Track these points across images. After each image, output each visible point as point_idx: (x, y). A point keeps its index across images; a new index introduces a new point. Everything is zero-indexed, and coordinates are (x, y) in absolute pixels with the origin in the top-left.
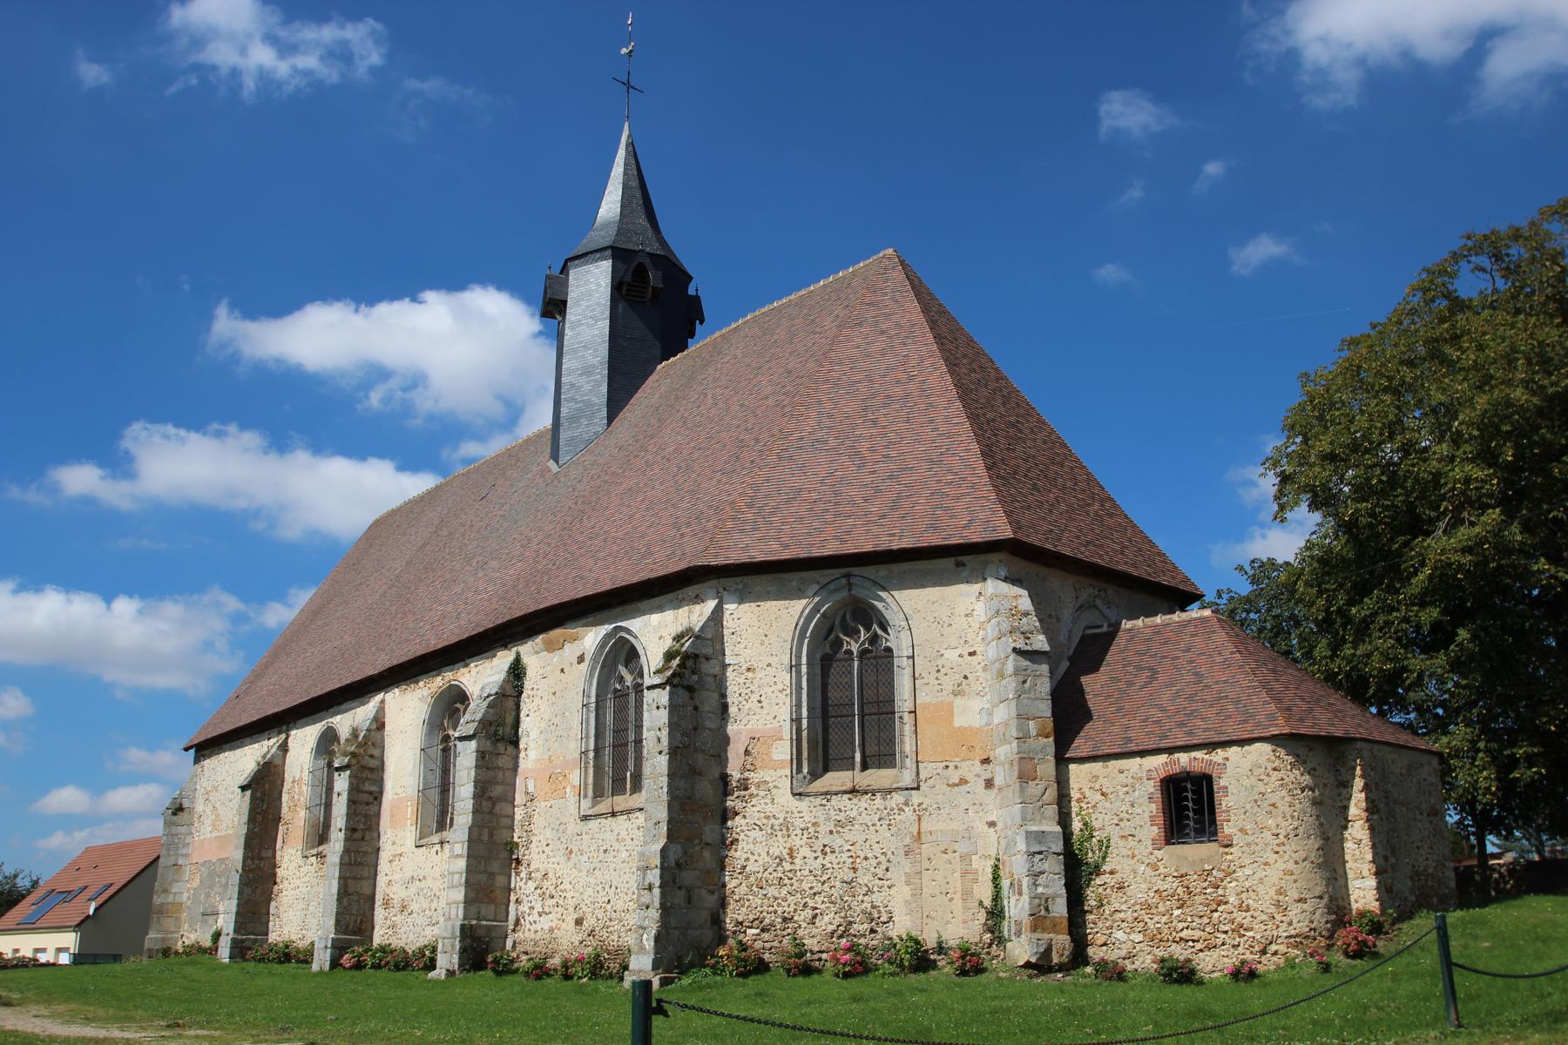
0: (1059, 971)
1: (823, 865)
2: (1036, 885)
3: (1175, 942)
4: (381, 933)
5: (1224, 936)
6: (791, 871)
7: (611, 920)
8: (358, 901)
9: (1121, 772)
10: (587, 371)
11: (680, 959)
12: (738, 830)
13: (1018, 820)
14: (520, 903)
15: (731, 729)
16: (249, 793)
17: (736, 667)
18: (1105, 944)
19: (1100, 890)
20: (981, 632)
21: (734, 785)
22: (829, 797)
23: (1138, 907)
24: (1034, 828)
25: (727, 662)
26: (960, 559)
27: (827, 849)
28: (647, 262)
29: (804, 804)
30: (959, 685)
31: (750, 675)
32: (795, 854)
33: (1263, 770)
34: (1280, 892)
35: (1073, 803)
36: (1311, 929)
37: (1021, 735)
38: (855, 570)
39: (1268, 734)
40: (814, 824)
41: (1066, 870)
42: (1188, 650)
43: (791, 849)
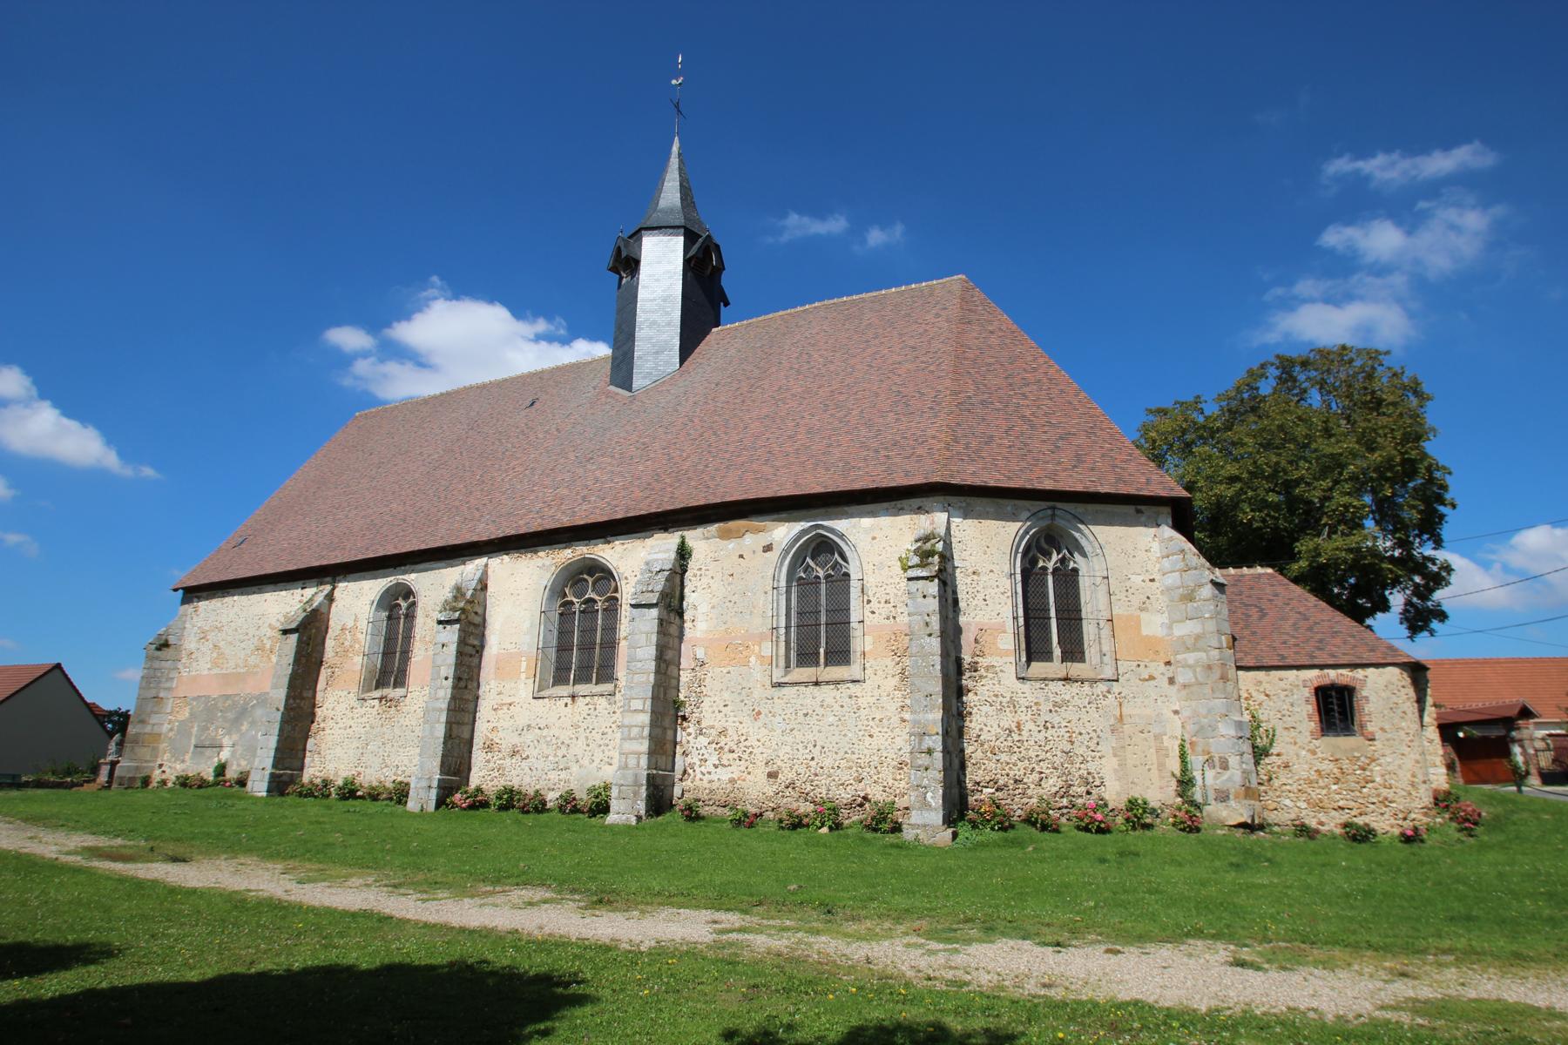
4: (481, 774)
6: (1019, 741)
7: (816, 775)
8: (459, 745)
9: (1281, 680)
12: (972, 704)
14: (687, 755)
15: (962, 620)
16: (294, 638)
19: (1269, 767)
23: (1302, 782)
26: (1139, 507)
29: (1026, 687)
30: (1144, 603)
31: (975, 577)
34: (1414, 776)
38: (1059, 505)
40: (1036, 704)
43: (1018, 723)
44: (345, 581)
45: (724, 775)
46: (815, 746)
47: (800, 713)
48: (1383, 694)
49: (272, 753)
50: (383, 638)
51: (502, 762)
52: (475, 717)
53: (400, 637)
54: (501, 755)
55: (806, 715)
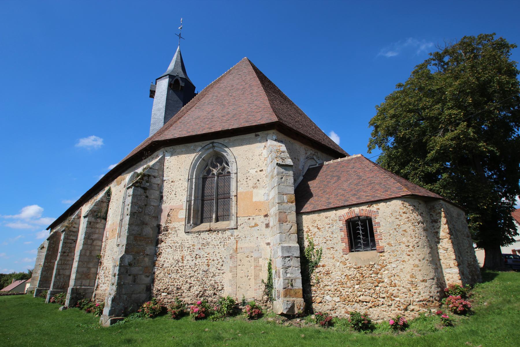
0: (298, 317)
1: (195, 264)
2: (286, 273)
3: (356, 302)
5: (383, 300)
6: (182, 266)
8: (64, 277)
9: (326, 218)
10: (159, 110)
11: (126, 309)
12: (162, 249)
13: (278, 241)
15: (164, 206)
17: (167, 181)
18: (321, 302)
19: (318, 275)
20: (265, 162)
21: (163, 229)
22: (200, 233)
24: (286, 245)
25: (164, 179)
26: (257, 133)
27: (198, 256)
28: (179, 79)
29: (189, 237)
31: (173, 184)
32: (184, 259)
33: (398, 213)
34: (412, 276)
35: (305, 233)
36: (430, 297)
37: (280, 202)
39: (400, 195)
40: (193, 245)
41: (301, 265)
42: (353, 168)
43: (182, 256)
48: (390, 220)
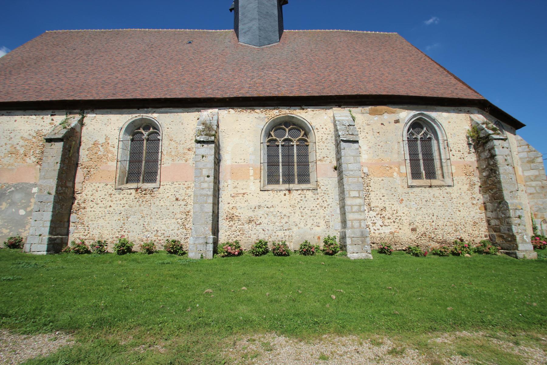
4: (228, 233)
44: (93, 113)
45: (386, 231)
46: (433, 216)
47: (424, 200)
49: (48, 224)
50: (129, 152)
51: (241, 226)
52: (218, 201)
53: (144, 152)
54: (240, 223)
55: (426, 201)
